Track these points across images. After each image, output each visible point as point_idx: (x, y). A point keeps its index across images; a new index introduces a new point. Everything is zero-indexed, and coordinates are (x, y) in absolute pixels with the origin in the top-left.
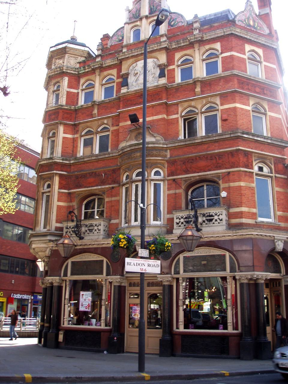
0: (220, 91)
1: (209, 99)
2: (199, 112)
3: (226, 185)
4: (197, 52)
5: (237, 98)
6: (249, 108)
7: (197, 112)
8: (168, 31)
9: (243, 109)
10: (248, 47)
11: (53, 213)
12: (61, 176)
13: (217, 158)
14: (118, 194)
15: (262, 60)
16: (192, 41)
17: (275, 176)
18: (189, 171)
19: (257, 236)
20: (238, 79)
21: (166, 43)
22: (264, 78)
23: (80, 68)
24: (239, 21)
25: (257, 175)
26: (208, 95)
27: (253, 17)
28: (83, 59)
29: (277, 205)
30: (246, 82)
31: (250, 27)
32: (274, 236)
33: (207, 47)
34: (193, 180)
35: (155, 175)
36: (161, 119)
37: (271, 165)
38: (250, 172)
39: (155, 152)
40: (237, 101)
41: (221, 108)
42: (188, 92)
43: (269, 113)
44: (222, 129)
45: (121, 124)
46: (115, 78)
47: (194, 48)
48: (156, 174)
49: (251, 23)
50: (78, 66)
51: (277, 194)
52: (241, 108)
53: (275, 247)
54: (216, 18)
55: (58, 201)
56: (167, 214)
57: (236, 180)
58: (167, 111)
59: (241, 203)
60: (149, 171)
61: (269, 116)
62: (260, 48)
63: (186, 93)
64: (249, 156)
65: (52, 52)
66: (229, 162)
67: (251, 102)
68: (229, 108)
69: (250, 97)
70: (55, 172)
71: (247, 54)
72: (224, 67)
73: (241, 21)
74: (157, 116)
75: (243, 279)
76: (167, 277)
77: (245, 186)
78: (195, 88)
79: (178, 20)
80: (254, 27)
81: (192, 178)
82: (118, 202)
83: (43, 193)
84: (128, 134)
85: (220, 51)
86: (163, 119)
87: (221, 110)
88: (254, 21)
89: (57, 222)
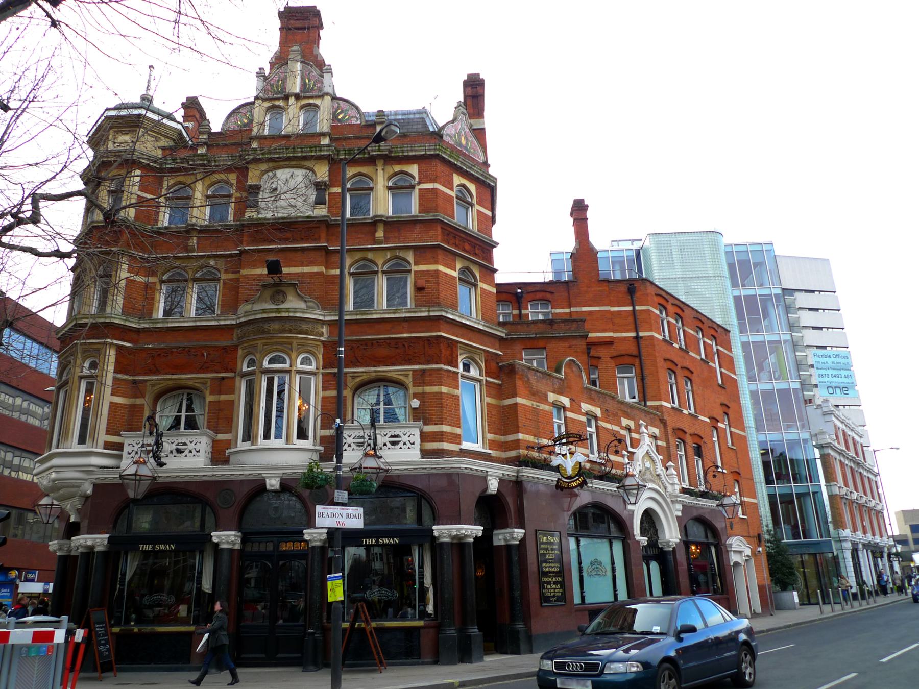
0: (414, 241)
1: (397, 253)
2: (380, 270)
3: (419, 390)
4: (380, 172)
5: (440, 257)
6: (455, 274)
7: (376, 269)
8: (332, 127)
9: (448, 274)
10: (457, 180)
11: (101, 415)
12: (119, 348)
13: (406, 346)
14: (232, 390)
15: (475, 201)
16: (374, 153)
17: (486, 380)
18: (359, 362)
19: (465, 471)
20: (442, 228)
21: (330, 148)
22: (476, 230)
23: (165, 157)
24: (447, 135)
25: (462, 376)
26: (396, 245)
27: (465, 133)
28: (171, 143)
29: (488, 424)
30: (452, 233)
31: (461, 147)
32: (487, 471)
33: (397, 168)
34: (365, 377)
35: (302, 364)
36: (317, 272)
37: (480, 362)
38: (454, 372)
39: (305, 327)
40: (440, 260)
41: (414, 268)
42: (363, 236)
43: (481, 285)
44: (415, 301)
45: (244, 272)
46: (233, 191)
47: (376, 165)
48: (305, 363)
49: (463, 141)
50: (159, 153)
51: (487, 406)
52: (444, 273)
53: (487, 488)
54: (407, 121)
55: (112, 395)
56: (321, 429)
57: (434, 382)
58: (327, 261)
59: (442, 418)
60: (293, 357)
61: (481, 288)
62: (472, 183)
63: (359, 236)
64: (454, 349)
65: (108, 118)
66: (424, 354)
67: (459, 266)
68: (427, 271)
69: (457, 257)
70: (109, 340)
71: (455, 189)
72: (422, 205)
73: (450, 136)
74: (309, 268)
75: (444, 537)
76: (229, 536)
77: (447, 394)
78: (375, 231)
79: (350, 112)
80: (465, 148)
81: (365, 374)
82: (232, 405)
83: (81, 378)
84: (259, 290)
85: (417, 179)
86: (320, 274)
87: (415, 271)
88: (466, 139)
89: (108, 432)
